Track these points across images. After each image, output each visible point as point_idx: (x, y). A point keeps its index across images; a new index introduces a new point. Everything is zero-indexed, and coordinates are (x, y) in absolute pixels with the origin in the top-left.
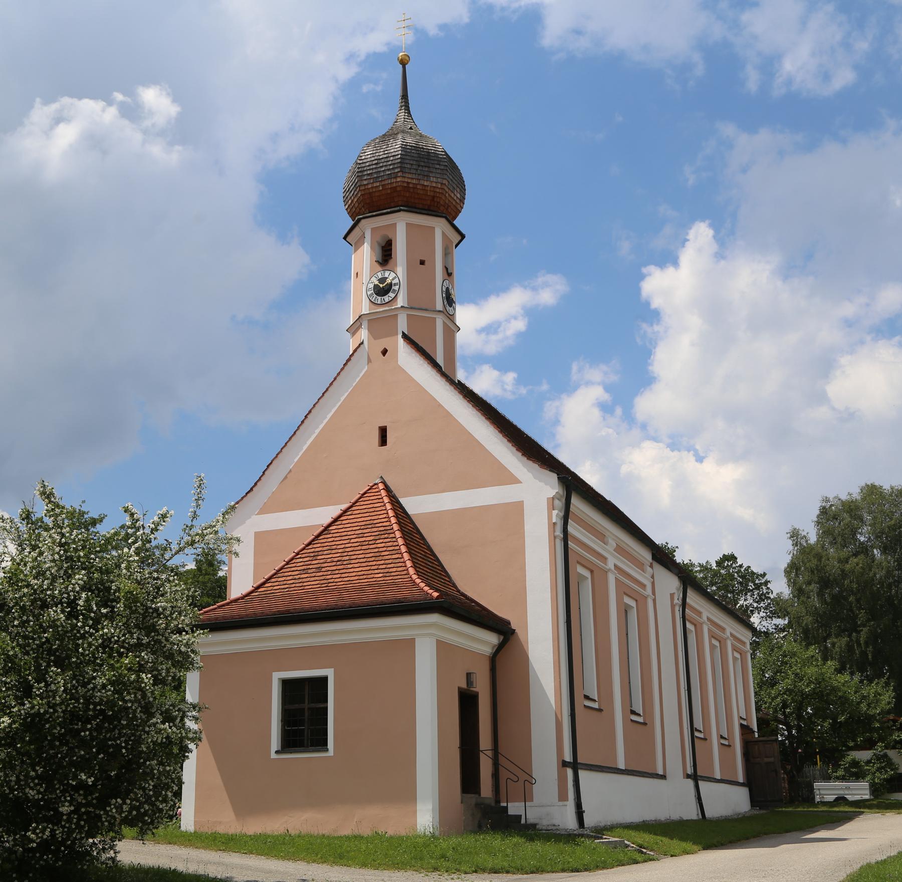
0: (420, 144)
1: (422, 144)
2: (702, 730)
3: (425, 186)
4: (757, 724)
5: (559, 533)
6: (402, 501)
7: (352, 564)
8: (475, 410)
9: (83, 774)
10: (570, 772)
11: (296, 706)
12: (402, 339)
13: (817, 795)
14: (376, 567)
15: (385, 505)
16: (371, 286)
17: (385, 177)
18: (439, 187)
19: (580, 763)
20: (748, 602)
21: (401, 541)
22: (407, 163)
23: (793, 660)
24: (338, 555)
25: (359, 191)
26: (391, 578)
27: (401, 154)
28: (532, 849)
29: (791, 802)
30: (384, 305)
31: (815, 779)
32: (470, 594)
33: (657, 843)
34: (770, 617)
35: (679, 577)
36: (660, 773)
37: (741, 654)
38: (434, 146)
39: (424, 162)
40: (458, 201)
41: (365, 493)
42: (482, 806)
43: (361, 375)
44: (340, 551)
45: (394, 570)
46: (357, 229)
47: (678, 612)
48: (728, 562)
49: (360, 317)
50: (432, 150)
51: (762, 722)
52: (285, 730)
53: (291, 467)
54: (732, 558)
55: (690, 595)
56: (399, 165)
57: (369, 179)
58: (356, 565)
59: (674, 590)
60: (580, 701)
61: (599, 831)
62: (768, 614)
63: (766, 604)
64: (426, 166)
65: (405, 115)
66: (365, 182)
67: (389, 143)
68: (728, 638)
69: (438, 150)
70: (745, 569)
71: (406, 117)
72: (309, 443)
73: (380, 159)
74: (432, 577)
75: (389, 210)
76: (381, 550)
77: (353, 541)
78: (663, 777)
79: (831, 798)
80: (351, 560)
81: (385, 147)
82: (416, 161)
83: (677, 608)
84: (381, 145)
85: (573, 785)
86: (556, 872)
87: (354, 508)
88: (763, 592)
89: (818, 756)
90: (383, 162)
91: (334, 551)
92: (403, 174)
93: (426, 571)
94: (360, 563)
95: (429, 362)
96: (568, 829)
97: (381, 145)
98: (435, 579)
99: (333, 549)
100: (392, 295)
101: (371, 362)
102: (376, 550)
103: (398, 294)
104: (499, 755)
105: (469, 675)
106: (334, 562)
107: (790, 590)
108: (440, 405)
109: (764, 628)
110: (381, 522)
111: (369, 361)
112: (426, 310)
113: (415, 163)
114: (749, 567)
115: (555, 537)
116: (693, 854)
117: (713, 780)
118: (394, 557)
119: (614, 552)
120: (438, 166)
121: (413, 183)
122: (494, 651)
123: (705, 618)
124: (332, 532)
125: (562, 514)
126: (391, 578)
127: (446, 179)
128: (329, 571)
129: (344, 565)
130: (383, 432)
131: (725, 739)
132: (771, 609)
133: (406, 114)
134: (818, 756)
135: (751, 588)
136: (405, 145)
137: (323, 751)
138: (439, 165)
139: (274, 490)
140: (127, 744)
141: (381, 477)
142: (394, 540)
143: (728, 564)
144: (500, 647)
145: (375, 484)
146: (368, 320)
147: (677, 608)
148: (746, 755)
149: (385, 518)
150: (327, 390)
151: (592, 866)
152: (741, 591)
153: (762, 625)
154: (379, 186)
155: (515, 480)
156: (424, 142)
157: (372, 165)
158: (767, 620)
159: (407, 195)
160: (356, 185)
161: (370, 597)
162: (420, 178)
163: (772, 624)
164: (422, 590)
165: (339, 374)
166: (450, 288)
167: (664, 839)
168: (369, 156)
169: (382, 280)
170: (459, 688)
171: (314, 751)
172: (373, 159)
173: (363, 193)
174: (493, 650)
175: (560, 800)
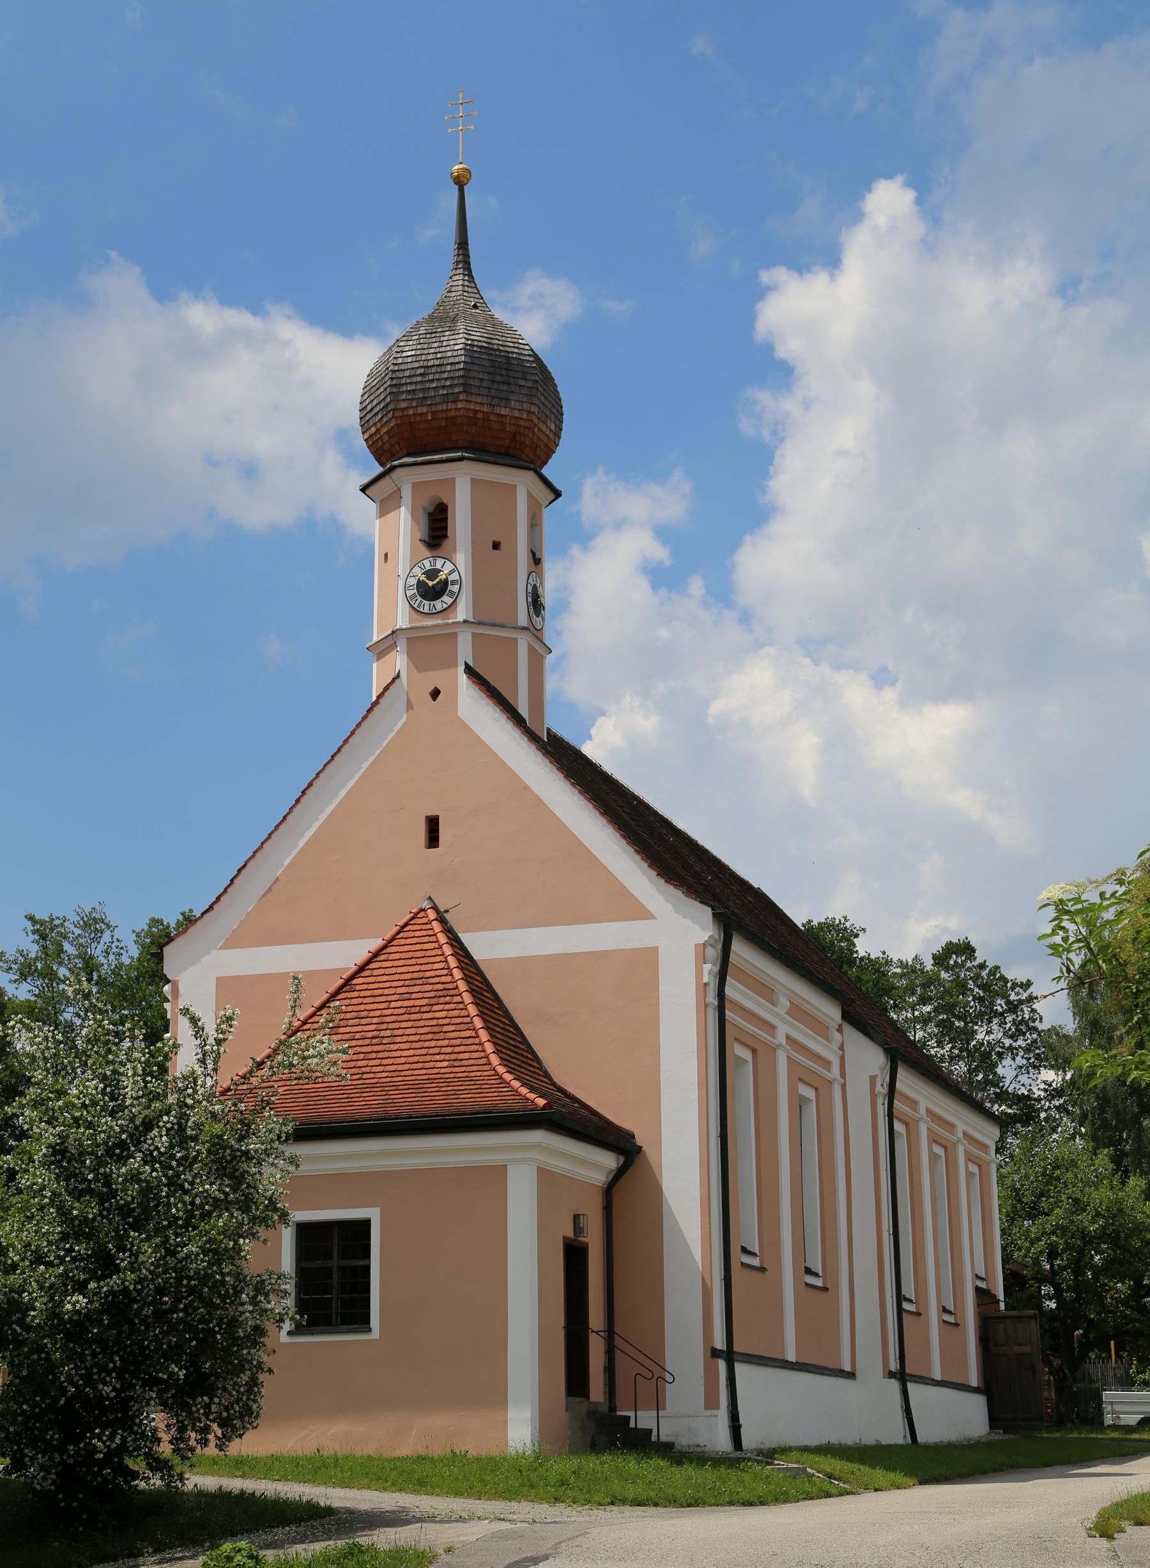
0: (494, 341)
1: (497, 342)
2: (913, 1298)
3: (502, 416)
4: (1004, 1284)
5: (712, 1000)
6: (465, 938)
7: (397, 1043)
8: (583, 798)
9: (173, 1366)
10: (722, 1365)
11: (318, 1264)
12: (465, 675)
13: (1108, 1413)
14: (436, 1050)
15: (440, 947)
16: (413, 581)
17: (438, 399)
18: (525, 417)
19: (737, 1353)
20: (992, 1037)
21: (472, 1010)
22: (474, 378)
23: (1070, 1175)
24: (373, 1027)
25: (391, 418)
26: (463, 1069)
27: (464, 362)
28: (680, 1477)
29: (1060, 1422)
30: (436, 615)
31: (1106, 1385)
32: (571, 1089)
33: (853, 1472)
34: (1035, 1067)
35: (885, 1050)
36: (846, 1369)
37: (980, 1166)
38: (516, 345)
39: (501, 375)
40: (551, 436)
41: (406, 925)
42: (598, 1415)
43: (396, 728)
44: (375, 1020)
45: (466, 1056)
46: (386, 481)
47: (882, 1107)
48: (957, 957)
49: (393, 632)
50: (513, 353)
51: (1013, 1280)
52: (301, 1299)
53: (278, 875)
54: (966, 949)
55: (902, 1078)
56: (461, 381)
57: (409, 399)
58: (404, 1046)
59: (876, 1071)
60: (737, 1257)
61: (768, 1455)
62: (1032, 1060)
63: (1029, 1041)
64: (503, 383)
65: (464, 280)
66: (403, 405)
67: (442, 339)
68: (959, 1141)
69: (523, 352)
70: (990, 970)
71: (466, 283)
72: (308, 835)
73: (428, 367)
74: (518, 1065)
75: (443, 456)
76: (441, 1022)
77: (393, 1005)
78: (851, 1375)
79: (1132, 1419)
80: (394, 1036)
81: (436, 345)
82: (488, 373)
83: (880, 1100)
84: (430, 341)
85: (727, 1385)
86: (722, 1505)
87: (389, 950)
88: (1023, 1018)
89: (1112, 1342)
90: (434, 373)
91: (364, 1021)
92: (467, 396)
93: (509, 1056)
94: (410, 1042)
95: (502, 707)
96: (719, 1451)
97: (430, 341)
98: (521, 1067)
99: (362, 1018)
100: (447, 599)
101: (412, 709)
102: (434, 1022)
103: (458, 600)
104: (616, 1335)
105: (576, 1218)
106: (366, 1038)
107: (1077, 1022)
108: (526, 788)
109: (1023, 1088)
110: (438, 976)
111: (410, 706)
112: (503, 626)
113: (486, 377)
114: (997, 968)
115: (706, 1006)
116: (905, 1488)
117: (918, 1380)
118: (464, 1034)
119: (787, 1016)
120: (523, 383)
121: (484, 412)
122: (610, 1178)
123: (923, 1111)
124: (358, 988)
125: (716, 969)
126: (463, 1069)
127: (535, 404)
128: (360, 1053)
129: (384, 1044)
130: (433, 824)
131: (950, 1312)
132: (1037, 1051)
133: (467, 278)
134: (1112, 1342)
135: (1000, 1010)
136: (470, 345)
137: (363, 1332)
138: (525, 379)
139: (249, 910)
140: (221, 1328)
141: (430, 898)
142: (461, 1006)
143: (956, 962)
144: (619, 1174)
145: (422, 910)
146: (408, 639)
147: (880, 1100)
148: (985, 1340)
149: (443, 969)
150: (339, 750)
151: (770, 1499)
152: (980, 1015)
153: (1019, 1082)
154: (427, 413)
155: (642, 913)
156: (500, 338)
157: (416, 375)
158: (1028, 1073)
159: (473, 431)
160: (386, 406)
161: (434, 1102)
162: (494, 403)
163: (1039, 1081)
164: (517, 1092)
165: (359, 725)
166: (538, 585)
167: (862, 1467)
168: (410, 359)
169: (432, 574)
170: (565, 1238)
171: (342, 1332)
172: (417, 365)
173: (399, 422)
174: (608, 1177)
175: (706, 1409)
